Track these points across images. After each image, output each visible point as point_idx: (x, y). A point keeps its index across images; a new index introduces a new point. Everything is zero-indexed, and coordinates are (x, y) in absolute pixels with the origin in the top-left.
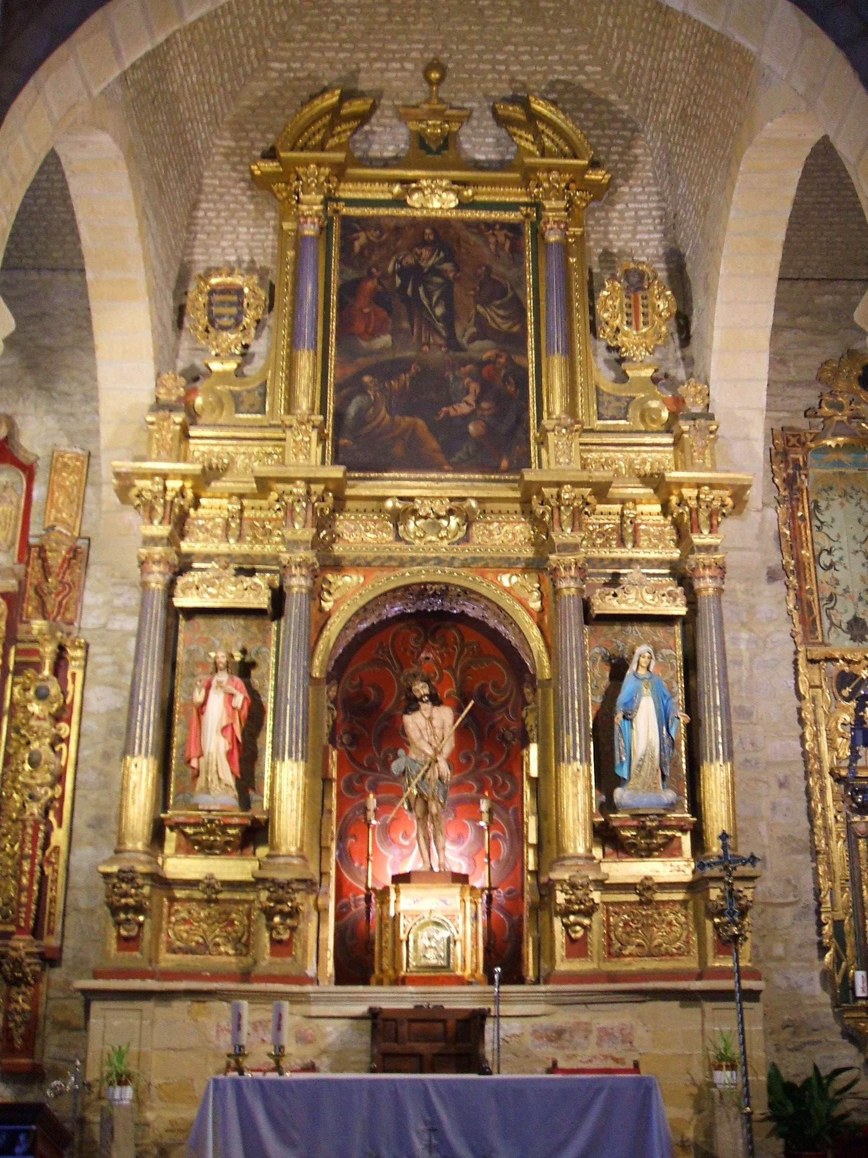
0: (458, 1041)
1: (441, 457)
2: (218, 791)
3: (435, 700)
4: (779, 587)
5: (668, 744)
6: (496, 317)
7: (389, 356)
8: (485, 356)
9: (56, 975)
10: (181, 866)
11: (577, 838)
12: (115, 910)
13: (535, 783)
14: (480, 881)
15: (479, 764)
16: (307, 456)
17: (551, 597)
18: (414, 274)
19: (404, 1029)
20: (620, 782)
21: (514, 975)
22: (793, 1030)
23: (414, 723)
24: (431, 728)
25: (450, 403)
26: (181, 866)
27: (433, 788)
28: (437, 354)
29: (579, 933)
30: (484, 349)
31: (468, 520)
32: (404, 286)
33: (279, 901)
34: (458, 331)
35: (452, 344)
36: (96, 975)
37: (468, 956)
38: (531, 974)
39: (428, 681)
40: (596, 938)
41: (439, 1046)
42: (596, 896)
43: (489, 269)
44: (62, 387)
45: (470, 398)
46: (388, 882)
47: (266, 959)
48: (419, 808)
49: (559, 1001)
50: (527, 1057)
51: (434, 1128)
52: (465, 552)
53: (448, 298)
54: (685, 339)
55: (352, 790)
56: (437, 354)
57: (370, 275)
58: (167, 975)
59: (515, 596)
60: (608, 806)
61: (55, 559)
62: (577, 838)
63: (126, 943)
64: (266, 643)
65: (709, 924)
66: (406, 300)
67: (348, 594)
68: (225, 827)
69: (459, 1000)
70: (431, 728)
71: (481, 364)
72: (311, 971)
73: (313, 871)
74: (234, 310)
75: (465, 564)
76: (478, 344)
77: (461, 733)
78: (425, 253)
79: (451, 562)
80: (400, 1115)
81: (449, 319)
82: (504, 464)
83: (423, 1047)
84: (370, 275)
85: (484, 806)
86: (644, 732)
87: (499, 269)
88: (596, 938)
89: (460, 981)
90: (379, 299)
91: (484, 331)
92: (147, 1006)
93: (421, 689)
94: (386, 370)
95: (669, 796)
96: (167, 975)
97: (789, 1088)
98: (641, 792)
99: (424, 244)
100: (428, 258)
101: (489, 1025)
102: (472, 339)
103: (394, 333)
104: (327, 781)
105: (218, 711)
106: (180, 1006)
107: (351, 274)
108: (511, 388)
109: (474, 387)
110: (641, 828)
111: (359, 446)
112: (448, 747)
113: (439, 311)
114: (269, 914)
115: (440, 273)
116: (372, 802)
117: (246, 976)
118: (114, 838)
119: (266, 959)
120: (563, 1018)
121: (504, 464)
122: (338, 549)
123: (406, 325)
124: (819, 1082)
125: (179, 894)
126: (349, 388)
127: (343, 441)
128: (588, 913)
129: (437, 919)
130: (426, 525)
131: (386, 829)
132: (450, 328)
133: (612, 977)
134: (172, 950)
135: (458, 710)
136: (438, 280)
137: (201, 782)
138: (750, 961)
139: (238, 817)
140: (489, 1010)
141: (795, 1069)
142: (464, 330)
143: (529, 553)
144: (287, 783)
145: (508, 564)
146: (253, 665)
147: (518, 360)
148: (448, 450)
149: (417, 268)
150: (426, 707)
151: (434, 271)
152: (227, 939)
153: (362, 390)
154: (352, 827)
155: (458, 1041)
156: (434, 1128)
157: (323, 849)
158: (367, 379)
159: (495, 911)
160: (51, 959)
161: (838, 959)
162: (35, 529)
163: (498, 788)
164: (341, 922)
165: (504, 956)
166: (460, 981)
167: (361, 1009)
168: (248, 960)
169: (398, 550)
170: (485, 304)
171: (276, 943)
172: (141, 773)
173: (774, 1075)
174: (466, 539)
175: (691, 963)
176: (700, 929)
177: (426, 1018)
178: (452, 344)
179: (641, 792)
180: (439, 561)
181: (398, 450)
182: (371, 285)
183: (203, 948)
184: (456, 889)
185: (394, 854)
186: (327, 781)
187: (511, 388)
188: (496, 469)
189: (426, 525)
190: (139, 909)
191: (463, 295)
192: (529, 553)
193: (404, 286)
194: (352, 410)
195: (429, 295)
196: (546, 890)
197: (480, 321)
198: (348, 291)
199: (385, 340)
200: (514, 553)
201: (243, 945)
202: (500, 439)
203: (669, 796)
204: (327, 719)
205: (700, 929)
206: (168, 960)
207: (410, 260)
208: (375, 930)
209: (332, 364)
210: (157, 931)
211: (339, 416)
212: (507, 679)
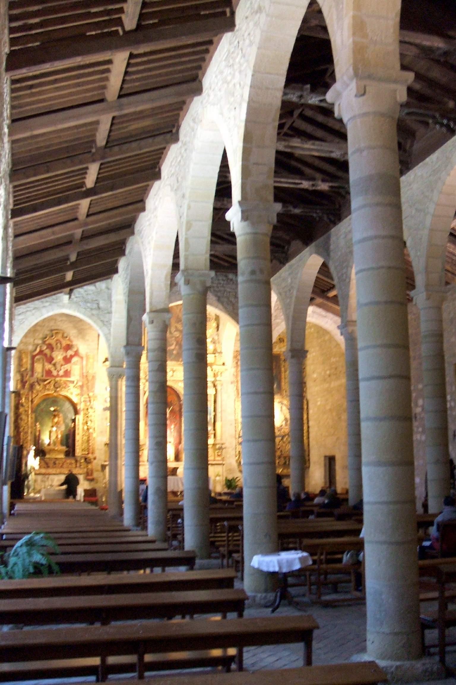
4: (233, 385)
9: (95, 461)
22: (230, 470)
31: (174, 371)
43: (178, 316)
44: (87, 338)
50: (247, 18)
54: (218, 330)
55: (378, 346)
61: (90, 378)
76: (176, 333)
97: (229, 480)
102: (175, 331)
109: (175, 343)
124: (233, 480)
138: (282, 543)
141: (230, 477)
160: (95, 459)
161: (239, 458)
162: (84, 371)
173: (226, 478)
176: (214, 453)
188: (178, 361)
197: (176, 327)
205: (214, 453)
212: (176, 399)
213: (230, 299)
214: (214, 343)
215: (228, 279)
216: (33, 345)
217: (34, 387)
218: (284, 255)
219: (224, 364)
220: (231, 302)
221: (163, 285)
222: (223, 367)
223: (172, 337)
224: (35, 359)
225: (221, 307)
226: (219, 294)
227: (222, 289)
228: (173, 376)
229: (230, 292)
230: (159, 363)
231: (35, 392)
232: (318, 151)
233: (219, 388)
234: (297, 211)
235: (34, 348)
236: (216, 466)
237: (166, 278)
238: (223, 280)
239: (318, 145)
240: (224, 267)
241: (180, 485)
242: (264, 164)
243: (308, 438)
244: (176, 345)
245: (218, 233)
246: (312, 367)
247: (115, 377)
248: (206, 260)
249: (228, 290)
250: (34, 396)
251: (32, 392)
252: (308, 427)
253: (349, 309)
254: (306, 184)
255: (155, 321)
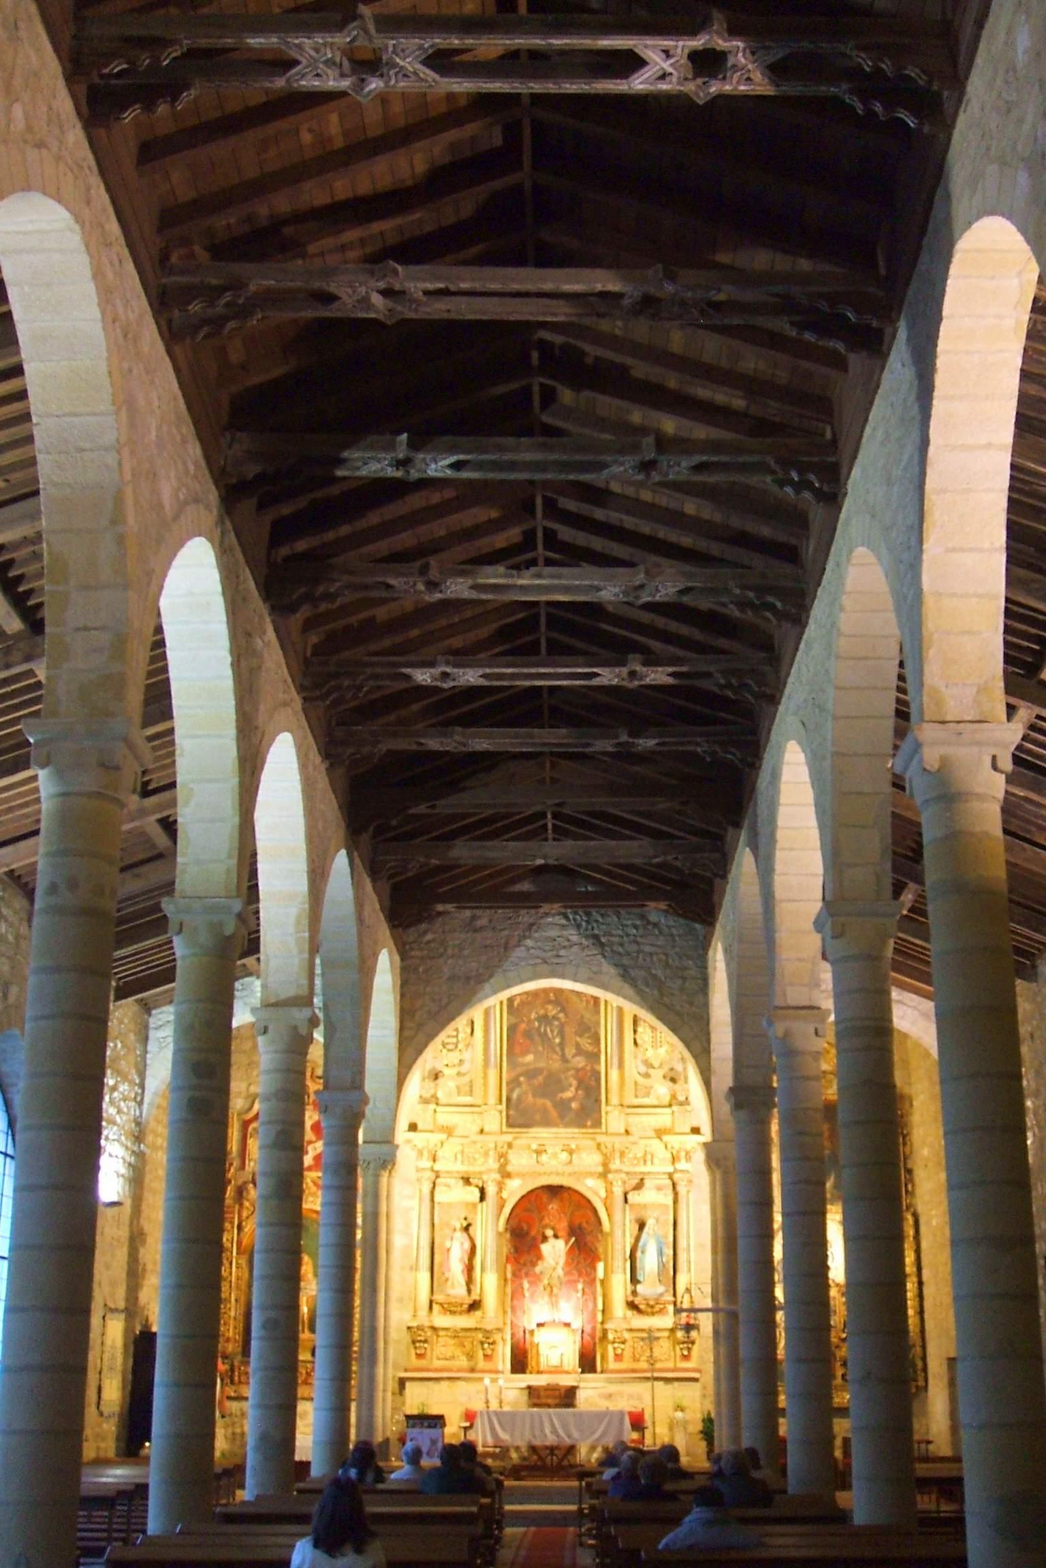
0: (567, 1397)
1: (558, 1120)
2: (457, 1289)
3: (556, 1236)
5: (662, 1266)
6: (586, 1043)
7: (532, 1067)
8: (581, 1065)
10: (441, 1320)
11: (619, 1308)
12: (414, 1342)
13: (602, 1282)
14: (577, 1324)
15: (578, 1263)
16: (494, 1119)
17: (609, 1192)
18: (544, 1019)
19: (542, 1393)
20: (639, 1282)
21: (592, 1369)
23: (545, 1248)
24: (554, 1251)
25: (563, 1091)
26: (441, 1320)
27: (555, 1282)
28: (556, 1065)
29: (619, 1351)
30: (580, 1062)
31: (571, 1152)
32: (540, 1026)
33: (487, 1338)
34: (567, 1051)
35: (564, 1059)
36: (406, 1370)
37: (572, 1359)
38: (599, 1368)
39: (553, 1228)
40: (627, 1355)
41: (557, 1401)
42: (627, 1335)
43: (582, 1017)
45: (573, 1089)
46: (534, 1326)
47: (481, 1364)
48: (549, 1289)
49: (610, 1381)
51: (553, 1425)
52: (570, 1169)
53: (562, 1033)
56: (556, 1065)
57: (523, 1021)
58: (436, 1370)
59: (592, 1188)
60: (634, 1293)
62: (619, 1308)
63: (419, 1356)
64: (476, 1213)
65: (678, 1348)
66: (540, 1034)
67: (515, 1189)
68: (461, 1305)
69: (566, 1381)
70: (554, 1251)
71: (578, 1070)
72: (500, 1368)
73: (500, 1325)
74: (454, 1040)
75: (570, 1174)
76: (578, 1059)
77: (570, 1252)
78: (550, 1007)
79: (563, 1174)
80: (542, 1423)
81: (562, 1045)
82: (589, 1123)
83: (550, 1401)
84: (523, 1021)
85: (580, 1286)
86: (649, 1262)
87: (587, 1016)
88: (627, 1355)
89: (567, 1372)
90: (528, 1034)
91: (580, 1051)
92: (430, 1384)
93: (549, 1233)
94: (531, 1074)
95: (661, 1289)
96: (436, 1370)
98: (649, 1288)
99: (550, 1002)
100: (552, 1010)
101: (578, 1392)
103: (536, 1053)
104: (506, 1280)
105: (457, 1248)
106: (444, 1384)
107: (514, 1020)
108: (593, 1083)
109: (574, 1083)
110: (648, 1304)
111: (519, 1117)
112: (562, 1261)
113: (557, 1040)
114: (482, 1343)
115: (558, 1019)
116: (526, 1285)
117: (472, 1370)
118: (411, 1308)
119: (481, 1364)
120: (613, 1388)
121: (589, 1123)
122: (509, 1168)
123: (540, 1048)
125: (441, 1333)
126: (514, 1083)
127: (511, 1112)
128: (623, 1342)
129: (557, 1351)
130: (552, 1155)
131: (532, 1295)
132: (563, 1050)
133: (634, 1371)
134: (439, 1359)
135: (567, 1243)
136: (556, 1023)
137: (449, 1283)
139: (468, 1301)
140: (242, 1487)
142: (570, 1051)
143: (600, 1169)
144: (489, 1284)
145: (590, 1174)
146: (469, 1225)
147: (596, 1067)
148: (562, 1117)
149: (545, 1017)
150: (552, 1241)
151: (554, 1017)
152: (463, 1353)
153: (519, 1084)
154: (517, 1293)
155: (567, 1397)
156: (553, 1425)
157: (505, 1312)
158: (522, 1079)
159: (585, 1336)
163: (588, 1275)
164: (255, 906)
165: (588, 1363)
166: (567, 1372)
167: (524, 1385)
168: (472, 1363)
169: (539, 1169)
170: (581, 1036)
171: (486, 1356)
172: (424, 1277)
174: (570, 1162)
175: (671, 1365)
177: (552, 1389)
178: (564, 1059)
179: (649, 1288)
180: (558, 1174)
181: (538, 1117)
182: (523, 1026)
183: (452, 1358)
184: (565, 1330)
185: (536, 1310)
186: (506, 1280)
187: (593, 1083)
188: (584, 1126)
189: (552, 1155)
190: (425, 1341)
191: (570, 1030)
192: (600, 1169)
193: (540, 1026)
194: (515, 1096)
195: (552, 1031)
196: (605, 1332)
197: (578, 1046)
198: (512, 1029)
199: (530, 1058)
200: (593, 1169)
201: (470, 1356)
202: (587, 1112)
203: (661, 1289)
204: (505, 1250)
206: (437, 1364)
207: (542, 1012)
208: (528, 1346)
209: (504, 1071)
210: (432, 1350)
211: (509, 1099)
213: (653, 972)
214: (673, 1080)
215: (649, 923)
216: (246, 1098)
217: (245, 1194)
218: (716, 855)
219: (627, 1132)
220: (655, 977)
221: (291, 941)
222: (625, 1139)
223: (568, 1070)
224: (250, 1129)
225: (630, 991)
226: (626, 961)
227: (634, 948)
228: (570, 1162)
229: (651, 954)
230: (279, 1128)
231: (247, 1204)
232: (567, 589)
233: (682, 1189)
234: (647, 743)
235: (247, 1106)
236: (676, 1384)
237: (298, 922)
238: (636, 927)
239: (552, 577)
240: (629, 895)
241: (548, 1431)
242: (103, 628)
243: (921, 1312)
244: (577, 1090)
245: (1012, 829)
246: (921, 1131)
247: (371, 1166)
248: (228, 871)
249: (647, 949)
250: (245, 1214)
251: (241, 1205)
252: (920, 1283)
253: (778, 977)
254: (608, 676)
255: (271, 1028)
